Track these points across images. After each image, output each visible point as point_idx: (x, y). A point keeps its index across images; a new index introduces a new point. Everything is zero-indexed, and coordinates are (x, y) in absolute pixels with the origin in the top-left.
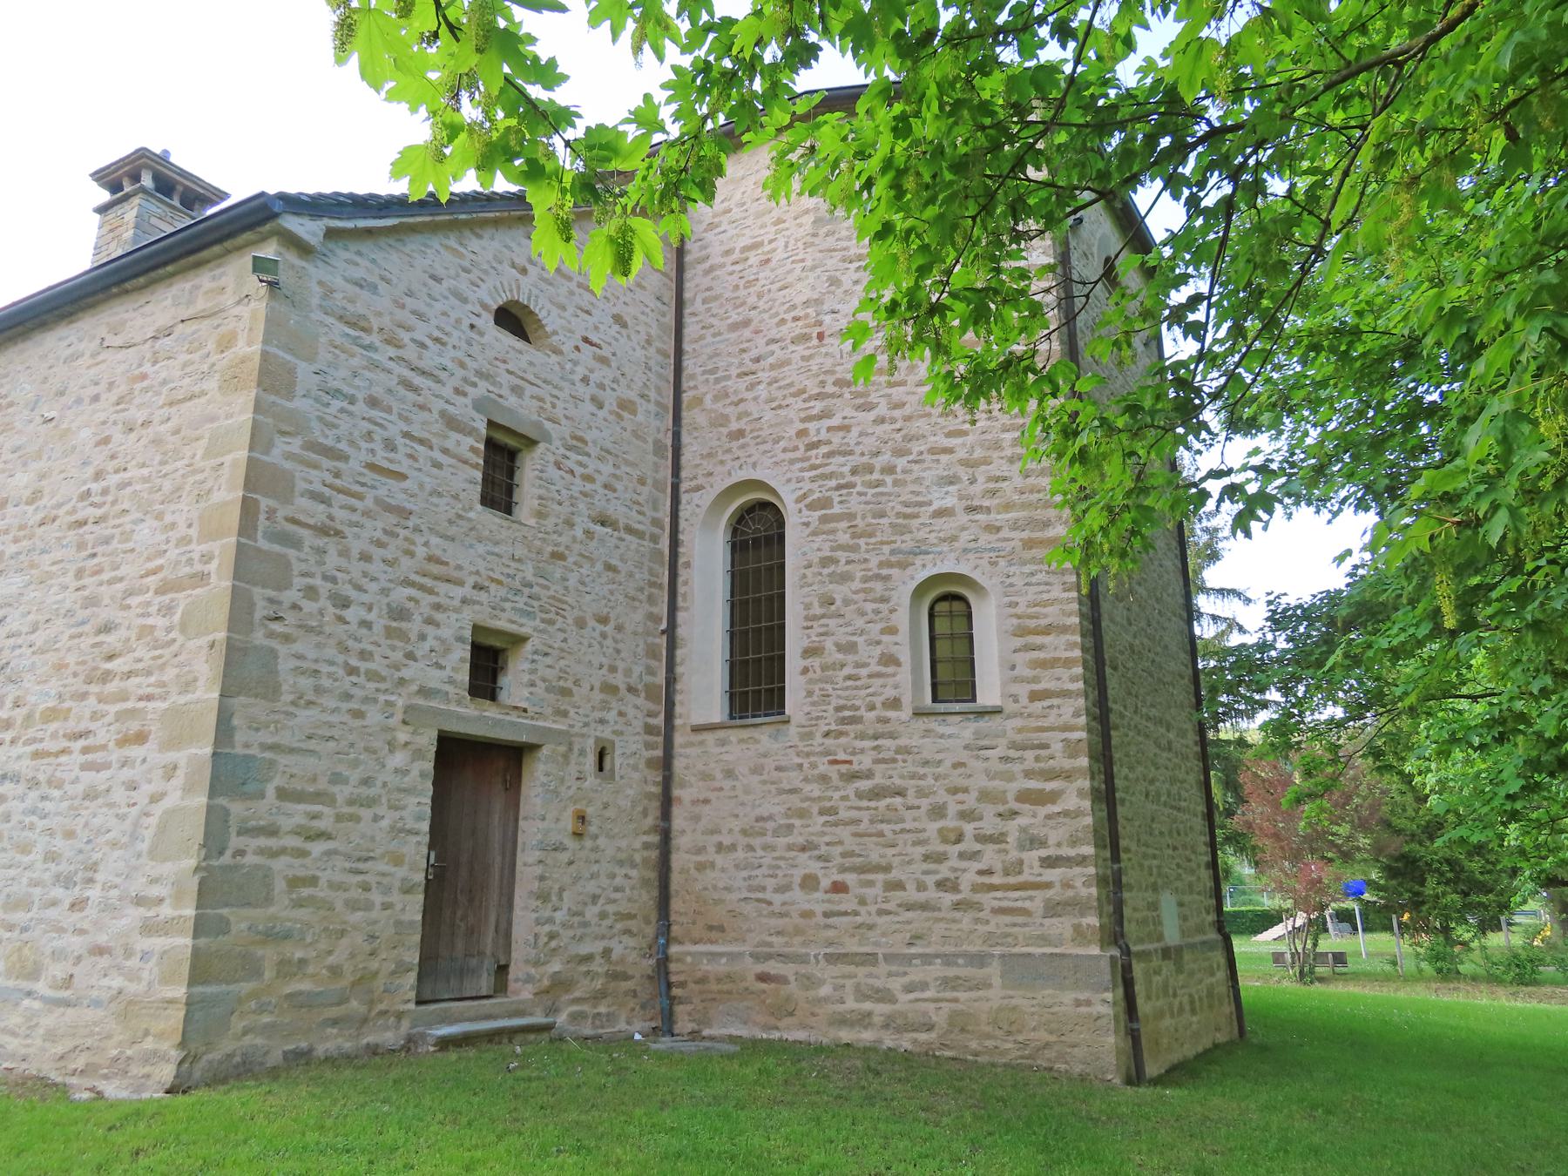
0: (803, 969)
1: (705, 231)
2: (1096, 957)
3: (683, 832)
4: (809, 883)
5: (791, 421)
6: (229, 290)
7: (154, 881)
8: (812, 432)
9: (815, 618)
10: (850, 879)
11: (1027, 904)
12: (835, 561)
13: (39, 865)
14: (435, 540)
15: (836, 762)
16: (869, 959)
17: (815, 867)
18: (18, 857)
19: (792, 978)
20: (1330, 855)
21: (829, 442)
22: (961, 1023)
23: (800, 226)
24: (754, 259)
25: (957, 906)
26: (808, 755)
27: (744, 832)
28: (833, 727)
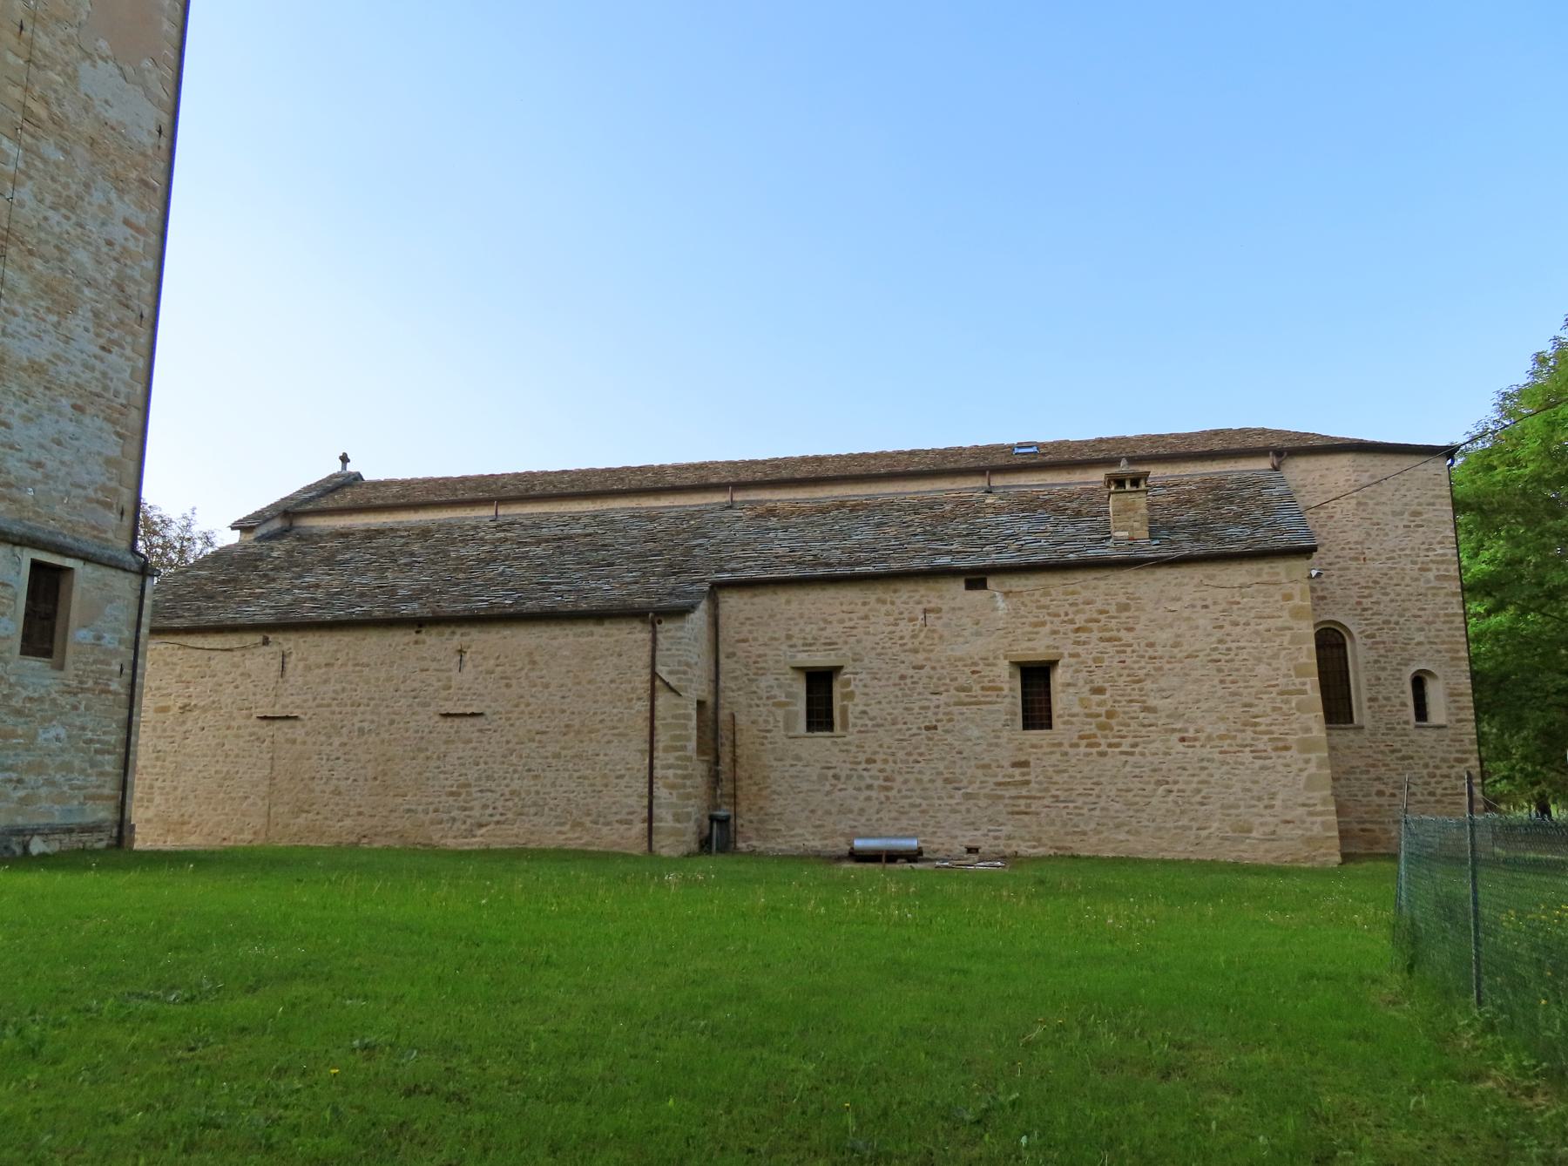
4: (1380, 793)
9: (1373, 685)
17: (1382, 787)
18: (1224, 790)
23: (1349, 503)
26: (1374, 742)
27: (1344, 773)
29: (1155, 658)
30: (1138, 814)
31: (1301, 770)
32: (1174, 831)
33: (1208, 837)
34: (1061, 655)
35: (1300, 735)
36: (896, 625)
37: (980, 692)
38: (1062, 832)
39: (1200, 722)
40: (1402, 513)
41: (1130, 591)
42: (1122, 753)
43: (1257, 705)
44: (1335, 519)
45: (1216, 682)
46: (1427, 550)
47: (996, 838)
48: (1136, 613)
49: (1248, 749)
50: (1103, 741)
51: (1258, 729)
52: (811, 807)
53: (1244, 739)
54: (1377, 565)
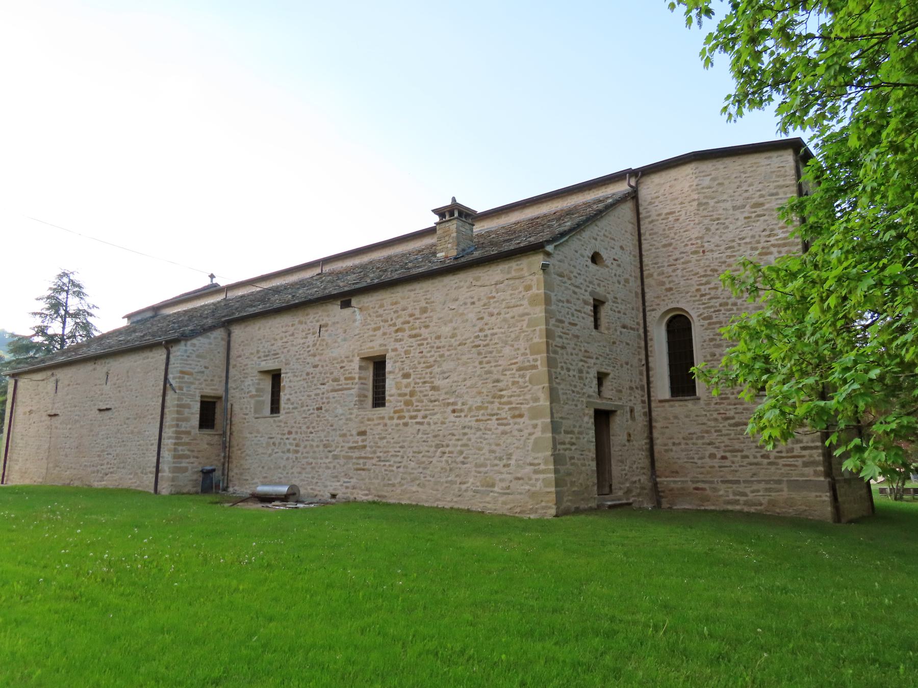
0: (713, 486)
1: (648, 205)
2: (823, 481)
3: (658, 438)
4: (712, 456)
5: (693, 285)
6: (525, 269)
7: (535, 458)
8: (703, 290)
9: (708, 361)
10: (728, 454)
11: (796, 463)
12: (715, 340)
13: (487, 454)
14: (586, 344)
15: (720, 414)
16: (738, 482)
17: (714, 451)
18: (477, 451)
19: (708, 489)
20: (912, 438)
21: (710, 294)
22: (772, 503)
23: (691, 206)
24: (671, 218)
25: (770, 464)
26: (709, 411)
27: (684, 438)
28: (718, 401)
29: (440, 348)
30: (425, 471)
31: (530, 434)
32: (447, 485)
33: (466, 491)
34: (387, 350)
35: (531, 404)
36: (306, 338)
37: (344, 381)
38: (382, 483)
39: (466, 397)
40: (744, 206)
41: (428, 297)
42: (417, 423)
43: (502, 381)
44: (681, 220)
45: (477, 364)
46: (769, 236)
47: (347, 488)
48: (431, 314)
49: (495, 417)
50: (407, 414)
51: (503, 400)
52: (263, 465)
53: (493, 409)
54: (716, 255)
